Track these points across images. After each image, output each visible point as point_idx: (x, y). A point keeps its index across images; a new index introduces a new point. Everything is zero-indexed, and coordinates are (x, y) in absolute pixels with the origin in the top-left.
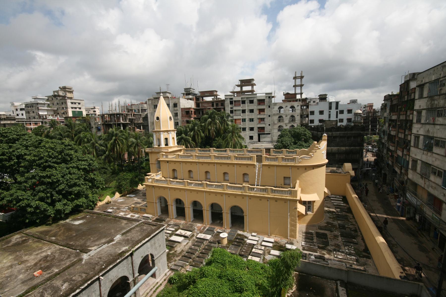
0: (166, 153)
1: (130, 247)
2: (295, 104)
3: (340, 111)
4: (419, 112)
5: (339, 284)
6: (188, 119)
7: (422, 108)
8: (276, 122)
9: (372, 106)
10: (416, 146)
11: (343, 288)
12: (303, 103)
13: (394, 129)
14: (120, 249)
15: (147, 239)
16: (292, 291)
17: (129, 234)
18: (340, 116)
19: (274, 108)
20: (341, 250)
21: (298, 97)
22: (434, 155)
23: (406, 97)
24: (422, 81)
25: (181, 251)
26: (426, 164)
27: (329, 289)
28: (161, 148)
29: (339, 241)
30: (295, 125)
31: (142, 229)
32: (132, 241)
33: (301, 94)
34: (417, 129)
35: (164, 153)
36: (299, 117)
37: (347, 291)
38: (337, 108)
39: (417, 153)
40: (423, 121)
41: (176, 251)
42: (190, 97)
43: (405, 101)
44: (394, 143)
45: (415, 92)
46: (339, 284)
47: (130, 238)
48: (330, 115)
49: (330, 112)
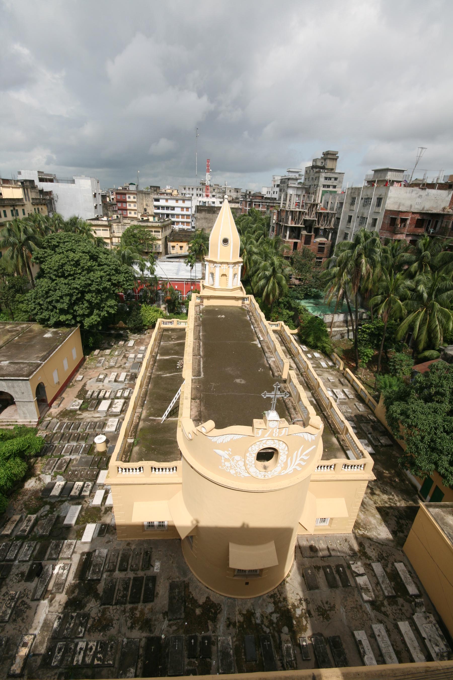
29: (124, 630)
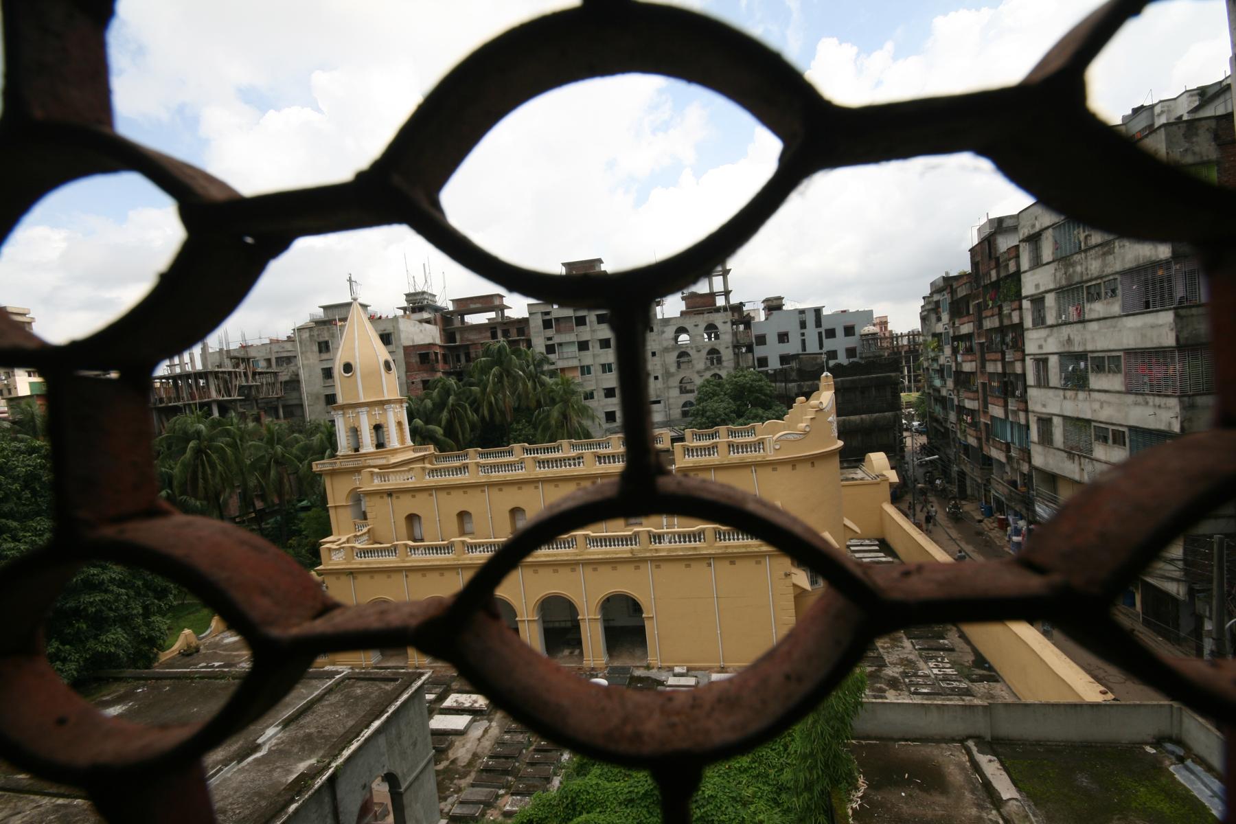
0: (380, 467)
1: (323, 756)
2: (718, 319)
3: (827, 331)
4: (1038, 301)
5: (974, 750)
6: (425, 376)
7: (1042, 289)
8: (673, 369)
9: (886, 323)
10: (1043, 383)
11: (989, 757)
12: (736, 316)
13: (969, 358)
14: (289, 772)
15: (376, 724)
16: (860, 794)
17: (308, 719)
18: (829, 345)
19: (663, 332)
20: (920, 673)
21: (720, 302)
22: (1095, 395)
23: (993, 273)
24: (1033, 226)
25: (469, 756)
26: (1077, 423)
27: (952, 767)
28: (365, 454)
29: (906, 651)
30: (723, 373)
31: (348, 697)
32: (324, 737)
33: (727, 293)
34: (1034, 342)
35: (376, 470)
36: (730, 351)
37: (1002, 763)
38: (818, 323)
39: (1047, 401)
40: (1051, 319)
41: (453, 762)
42: (426, 315)
43: (992, 283)
44: (977, 391)
45: (1017, 257)
46: (974, 750)
47: (313, 730)
48: (803, 342)
49: (803, 334)
